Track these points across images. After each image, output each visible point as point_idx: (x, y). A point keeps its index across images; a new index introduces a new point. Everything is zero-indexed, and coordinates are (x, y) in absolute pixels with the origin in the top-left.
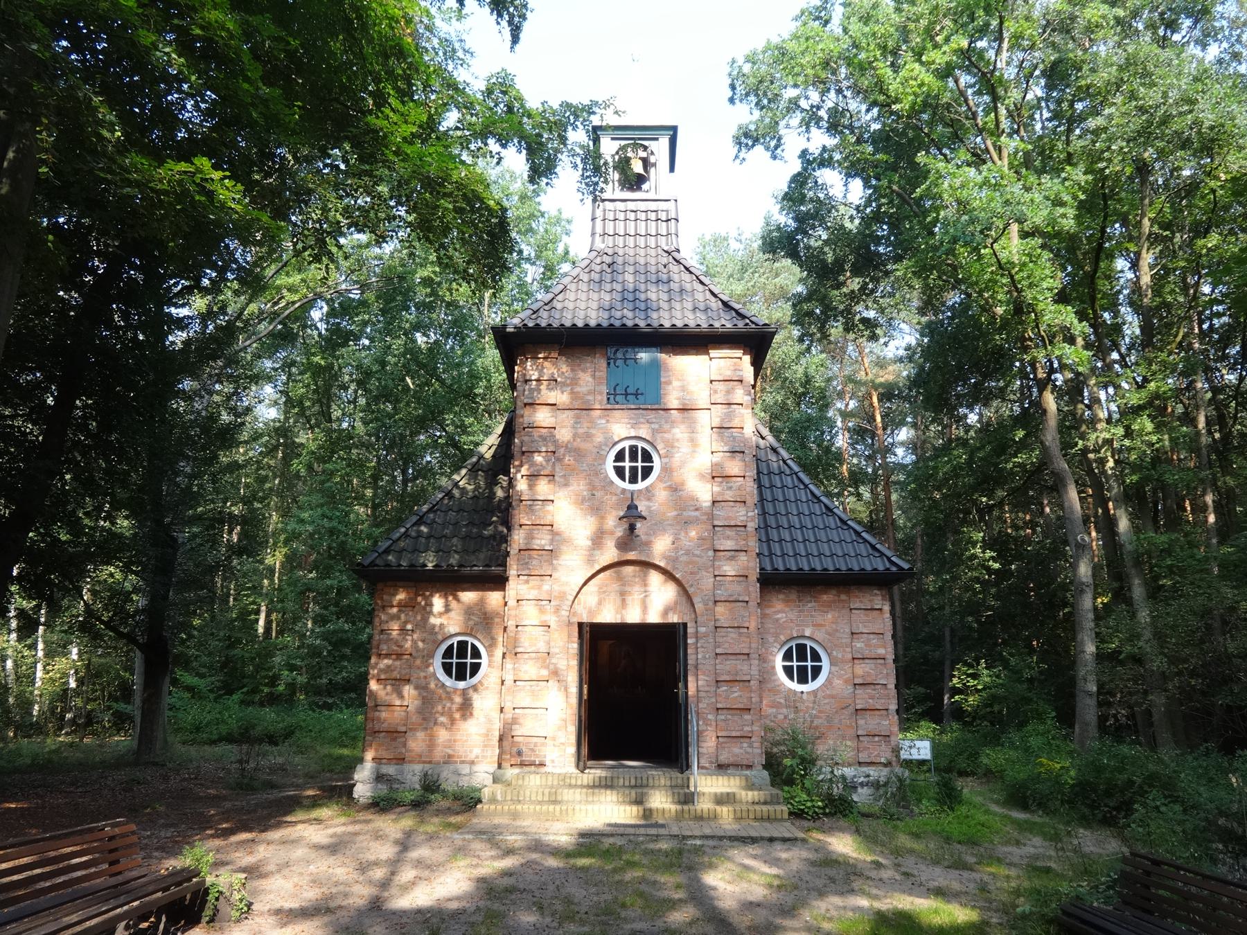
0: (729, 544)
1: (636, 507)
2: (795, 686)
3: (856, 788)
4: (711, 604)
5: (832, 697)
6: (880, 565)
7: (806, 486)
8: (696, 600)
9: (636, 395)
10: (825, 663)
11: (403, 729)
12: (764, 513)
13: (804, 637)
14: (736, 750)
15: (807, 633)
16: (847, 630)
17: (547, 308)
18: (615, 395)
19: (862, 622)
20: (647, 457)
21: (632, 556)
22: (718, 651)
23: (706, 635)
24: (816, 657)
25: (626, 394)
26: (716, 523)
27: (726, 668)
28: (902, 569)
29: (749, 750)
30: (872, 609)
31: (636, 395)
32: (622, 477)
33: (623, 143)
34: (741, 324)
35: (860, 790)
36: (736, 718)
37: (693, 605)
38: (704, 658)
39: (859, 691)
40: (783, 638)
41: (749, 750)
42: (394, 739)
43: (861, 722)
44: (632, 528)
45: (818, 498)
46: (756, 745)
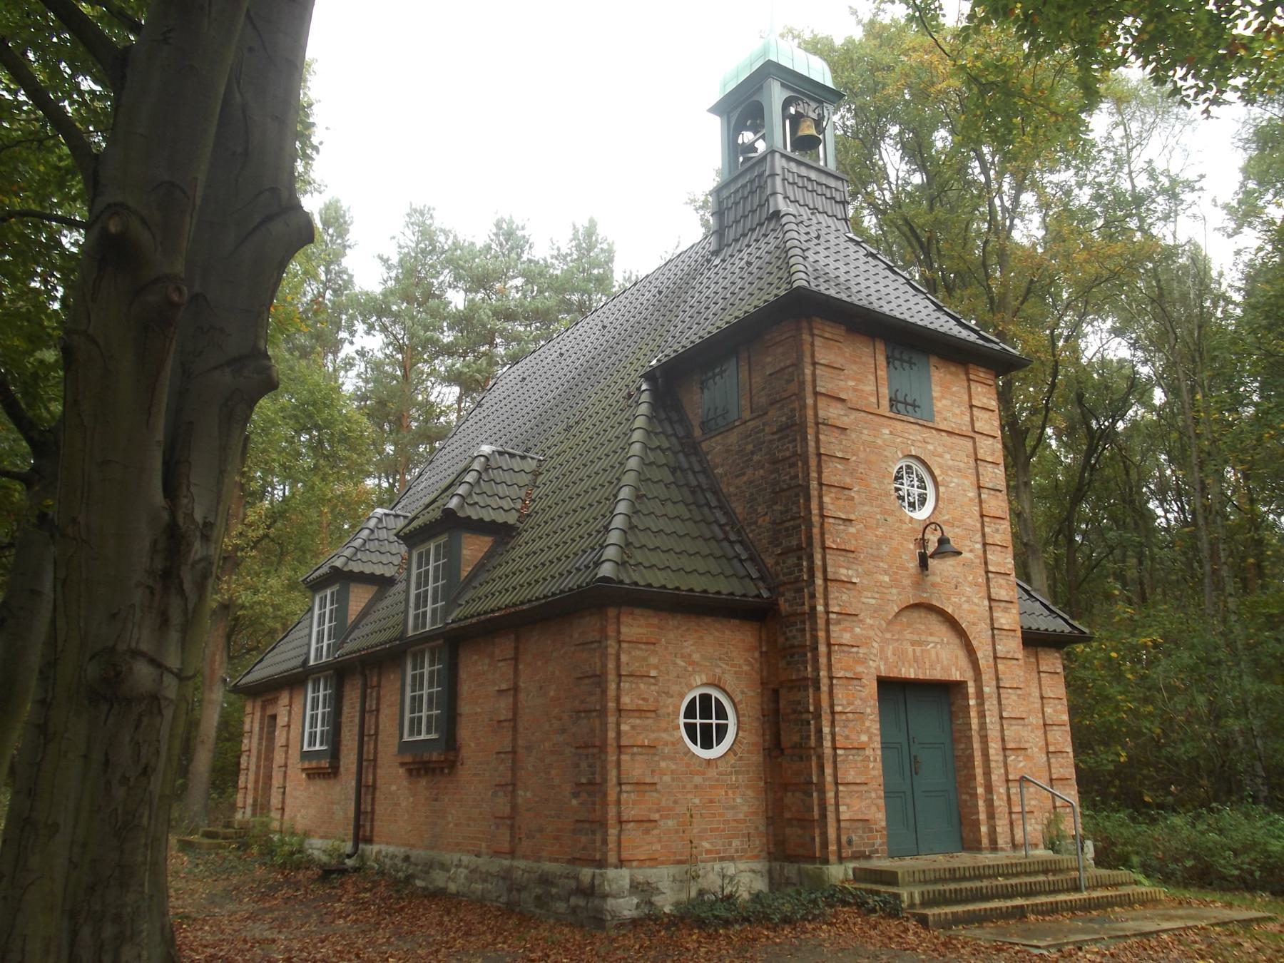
21: (924, 597)
31: (914, 406)
38: (991, 722)
42: (647, 832)
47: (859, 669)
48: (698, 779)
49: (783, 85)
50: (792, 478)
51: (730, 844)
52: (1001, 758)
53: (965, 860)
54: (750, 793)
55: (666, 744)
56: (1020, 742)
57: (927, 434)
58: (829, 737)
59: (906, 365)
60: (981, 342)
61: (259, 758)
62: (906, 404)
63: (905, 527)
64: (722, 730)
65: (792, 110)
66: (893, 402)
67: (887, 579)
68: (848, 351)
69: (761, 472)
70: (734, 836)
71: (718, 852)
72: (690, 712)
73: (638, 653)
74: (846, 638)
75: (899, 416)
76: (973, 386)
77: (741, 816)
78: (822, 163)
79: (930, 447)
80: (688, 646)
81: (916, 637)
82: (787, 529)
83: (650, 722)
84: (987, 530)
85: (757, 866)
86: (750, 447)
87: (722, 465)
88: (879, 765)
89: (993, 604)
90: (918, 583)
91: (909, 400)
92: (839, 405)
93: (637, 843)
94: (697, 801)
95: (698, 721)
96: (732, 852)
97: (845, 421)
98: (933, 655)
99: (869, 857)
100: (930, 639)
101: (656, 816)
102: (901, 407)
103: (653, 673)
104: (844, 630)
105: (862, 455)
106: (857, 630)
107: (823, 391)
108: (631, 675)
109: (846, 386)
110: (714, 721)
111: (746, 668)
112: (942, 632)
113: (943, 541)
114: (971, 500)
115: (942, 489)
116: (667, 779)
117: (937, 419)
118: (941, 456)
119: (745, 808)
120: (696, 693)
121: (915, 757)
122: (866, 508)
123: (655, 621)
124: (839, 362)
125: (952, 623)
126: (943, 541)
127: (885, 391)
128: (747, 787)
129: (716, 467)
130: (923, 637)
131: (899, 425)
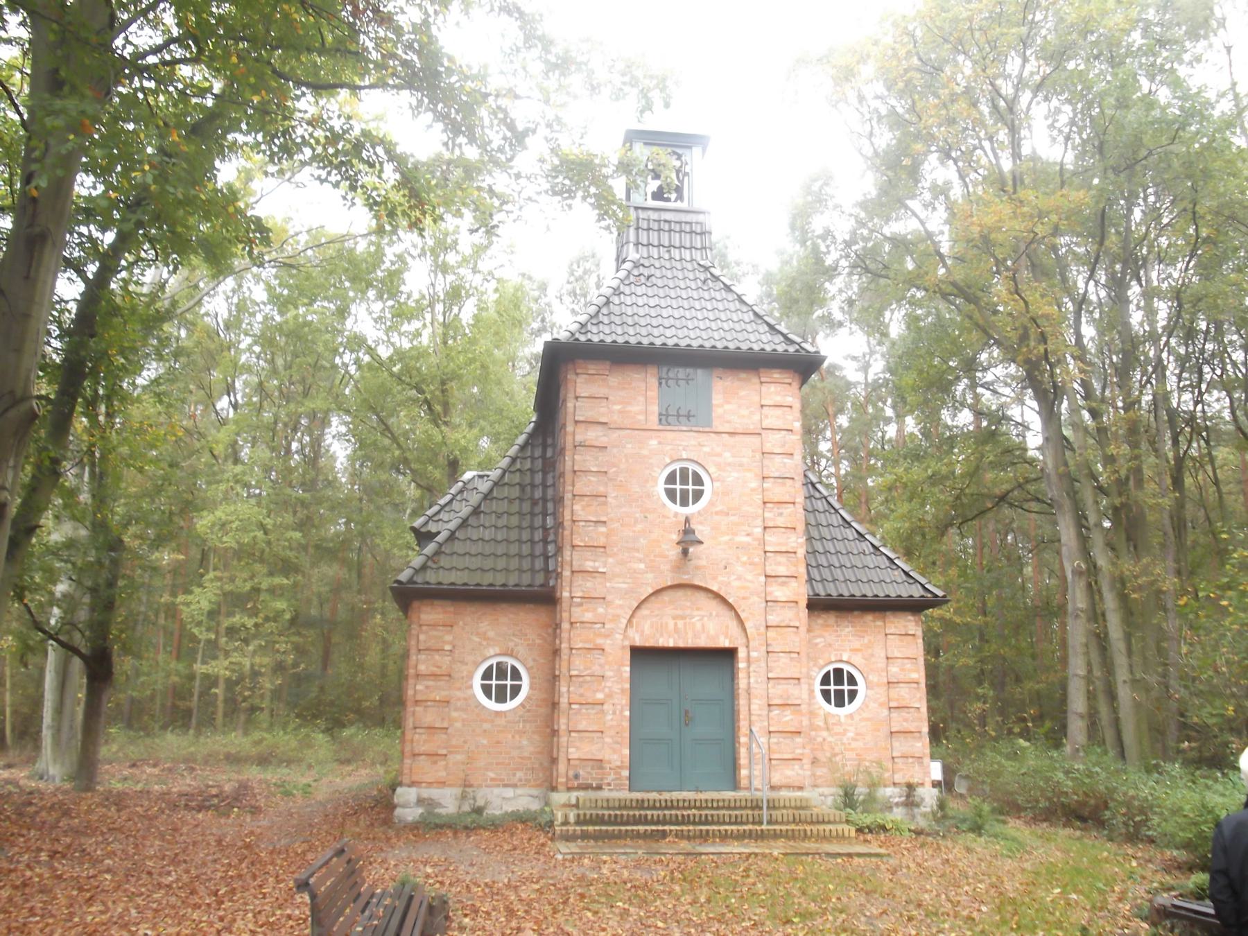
0: (782, 570)
1: (693, 532)
2: (492, 705)
3: (891, 807)
4: (763, 629)
5: (868, 719)
6: (917, 592)
7: (836, 511)
8: (748, 625)
9: (688, 416)
10: (861, 687)
11: (444, 752)
12: (810, 539)
13: (841, 661)
14: (789, 772)
15: (845, 658)
16: (883, 655)
17: (594, 321)
18: (667, 415)
19: (897, 648)
20: (698, 480)
21: (685, 579)
22: (770, 675)
23: (758, 660)
24: (852, 681)
25: (678, 416)
26: (768, 549)
27: (777, 691)
28: (937, 596)
29: (801, 772)
30: (907, 635)
31: (688, 416)
32: (673, 500)
33: (1083, 320)
34: (791, 349)
35: (895, 810)
36: (787, 741)
37: (744, 630)
38: (757, 682)
39: (894, 715)
40: (821, 662)
41: (801, 772)
42: (435, 763)
43: (896, 744)
44: (685, 552)
45: (848, 523)
46: (806, 767)
48: (486, 726)
51: (514, 775)
53: (729, 795)
54: (536, 737)
55: (459, 699)
56: (788, 698)
57: (703, 438)
58: (566, 695)
63: (667, 521)
64: (516, 690)
67: (642, 566)
68: (614, 380)
70: (518, 769)
71: (502, 780)
72: (853, 694)
73: (434, 633)
75: (669, 428)
77: (526, 754)
79: (706, 449)
80: (484, 626)
81: (679, 612)
83: (442, 683)
85: (535, 792)
90: (679, 568)
92: (600, 428)
93: (425, 769)
94: (485, 742)
95: (494, 682)
96: (515, 780)
97: (603, 441)
98: (698, 625)
99: (599, 788)
100: (696, 613)
104: (587, 610)
105: (623, 466)
106: (601, 610)
107: (581, 419)
108: (427, 650)
109: (610, 411)
110: (509, 682)
111: (538, 641)
112: (713, 606)
114: (753, 490)
118: (719, 455)
119: (532, 749)
120: (494, 661)
121: (686, 712)
122: (624, 510)
123: (452, 609)
124: (602, 391)
127: (655, 409)
128: (534, 732)
130: (688, 612)
131: (670, 435)
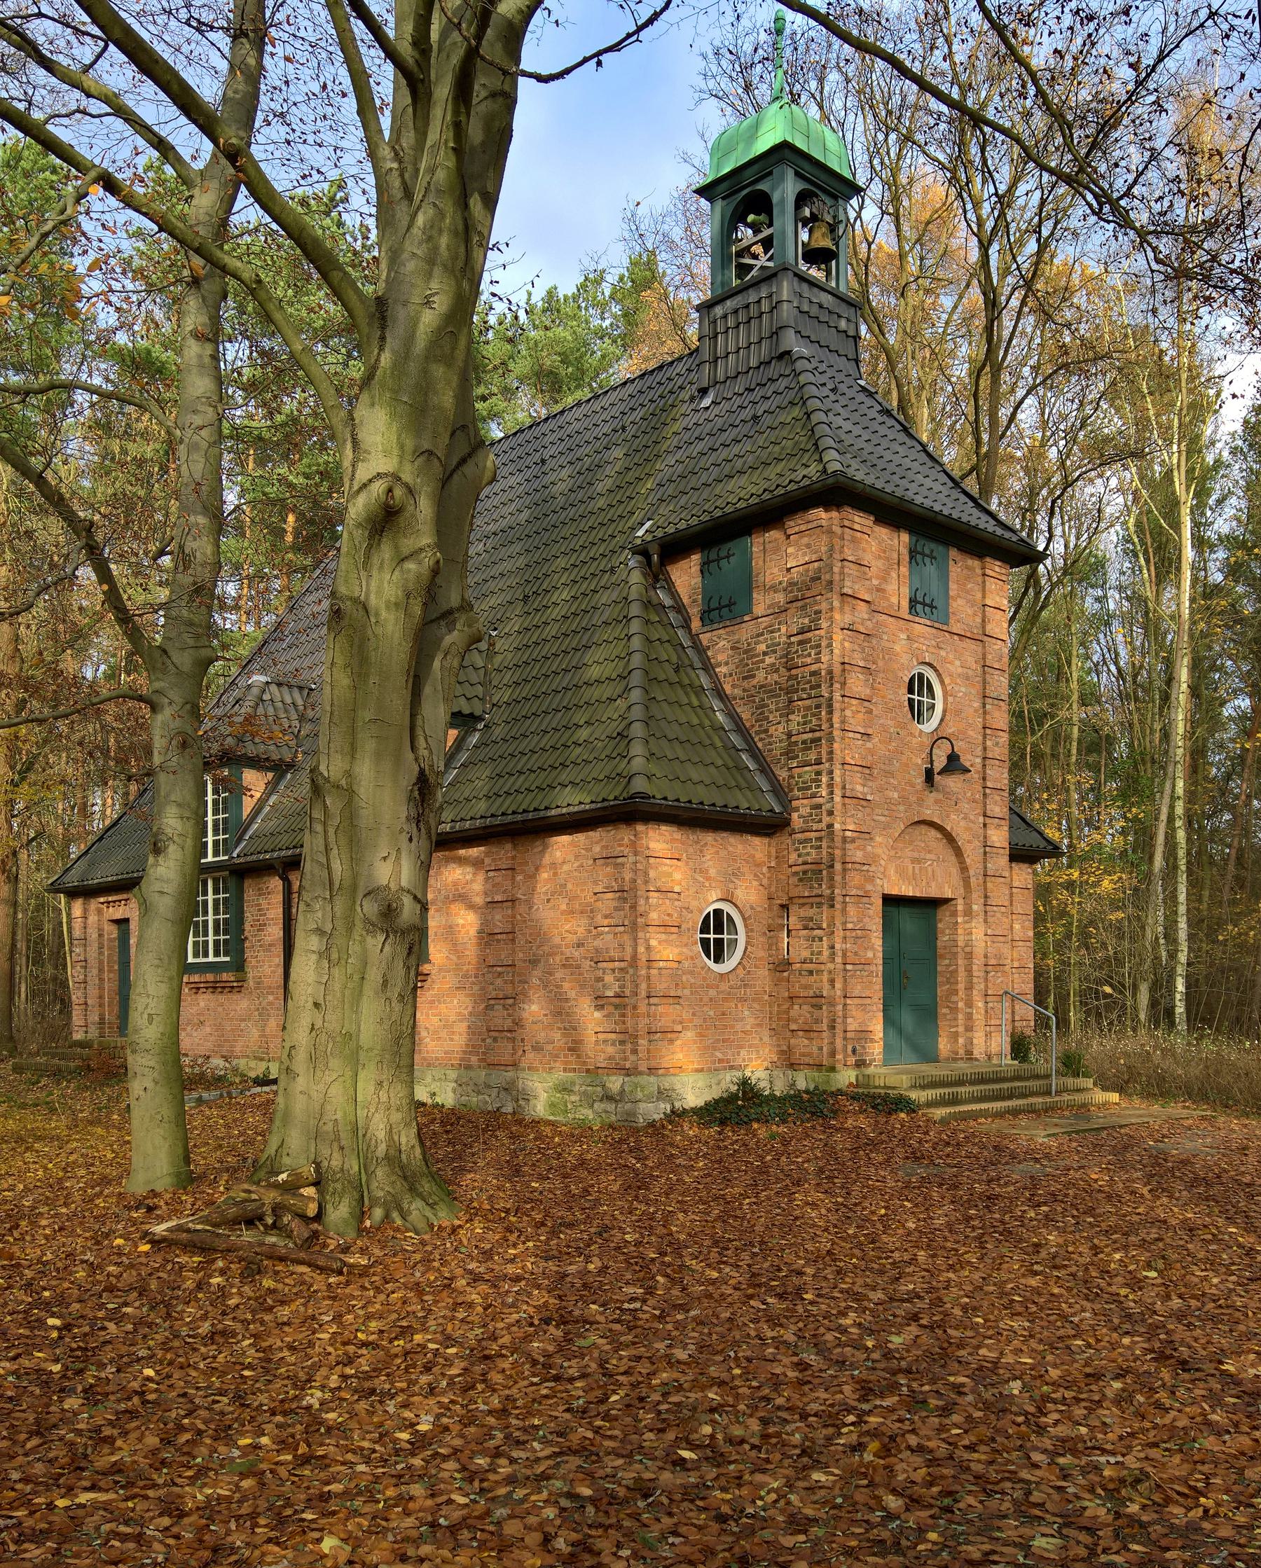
31: (932, 607)
47: (869, 887)
48: (712, 993)
49: (797, 174)
50: (812, 688)
52: (982, 974)
59: (927, 560)
60: (999, 531)
61: (101, 970)
62: (924, 604)
65: (807, 212)
66: (913, 602)
69: (775, 676)
72: (705, 929)
74: (859, 856)
76: (989, 581)
78: (833, 284)
81: (916, 855)
82: (804, 742)
84: (989, 743)
86: (762, 647)
87: (727, 664)
88: (880, 980)
89: (988, 821)
91: (928, 601)
95: (712, 936)
100: (928, 856)
101: (679, 1028)
102: (919, 607)
103: (677, 889)
105: (881, 663)
110: (725, 936)
113: (953, 758)
115: (950, 699)
116: (687, 992)
117: (952, 621)
120: (711, 909)
125: (949, 838)
126: (953, 758)
129: (719, 665)
